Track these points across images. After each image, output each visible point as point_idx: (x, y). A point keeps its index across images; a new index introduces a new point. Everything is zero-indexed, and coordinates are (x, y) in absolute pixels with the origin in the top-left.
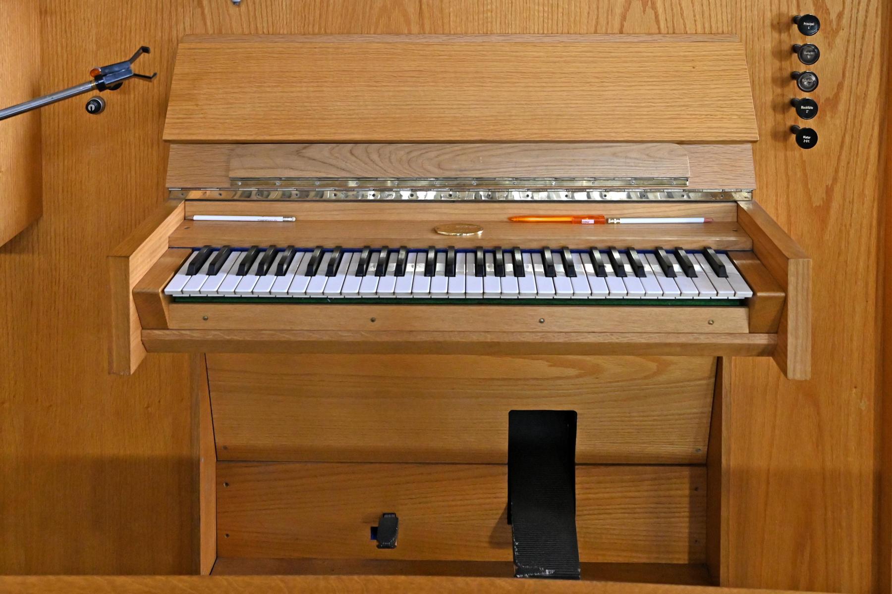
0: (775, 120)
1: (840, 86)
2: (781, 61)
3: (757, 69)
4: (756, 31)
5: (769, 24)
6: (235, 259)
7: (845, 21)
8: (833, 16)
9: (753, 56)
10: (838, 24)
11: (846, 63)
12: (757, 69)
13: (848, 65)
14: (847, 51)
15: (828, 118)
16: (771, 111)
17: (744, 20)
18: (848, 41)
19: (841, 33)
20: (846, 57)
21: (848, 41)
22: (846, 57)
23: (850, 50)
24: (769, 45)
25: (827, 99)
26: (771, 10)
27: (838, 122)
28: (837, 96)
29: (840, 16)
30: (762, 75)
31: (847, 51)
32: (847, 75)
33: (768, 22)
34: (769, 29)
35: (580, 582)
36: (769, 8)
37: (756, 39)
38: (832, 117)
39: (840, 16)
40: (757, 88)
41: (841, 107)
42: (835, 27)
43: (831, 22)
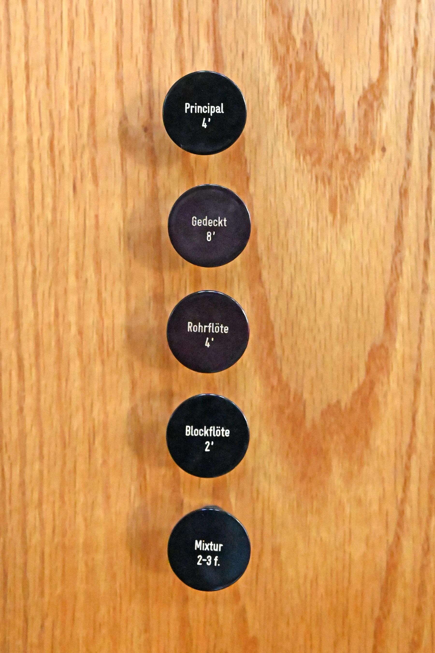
0: (142, 489)
1: (378, 356)
2: (159, 269)
3: (73, 299)
4: (67, 160)
5: (114, 132)
6: (416, 638)
7: (388, 121)
8: (347, 101)
9: (56, 251)
10: (365, 132)
11: (396, 271)
12: (73, 299)
13: (405, 282)
14: (399, 228)
15: (336, 479)
16: (124, 455)
17: (20, 117)
18: (404, 193)
19: (376, 165)
20: (397, 251)
21: (404, 193)
22: (397, 251)
23: (411, 223)
24: (117, 209)
25: (332, 410)
26: (120, 82)
27: (372, 493)
28: (366, 396)
29: (372, 97)
30: (91, 318)
31: (399, 228)
32: (402, 318)
33: (109, 125)
34: (114, 150)
35: (180, 148)
36: (110, 74)
37: (68, 189)
38: (349, 478)
39: (372, 97)
40: (75, 367)
41: (384, 437)
42: (352, 141)
43: (339, 121)
